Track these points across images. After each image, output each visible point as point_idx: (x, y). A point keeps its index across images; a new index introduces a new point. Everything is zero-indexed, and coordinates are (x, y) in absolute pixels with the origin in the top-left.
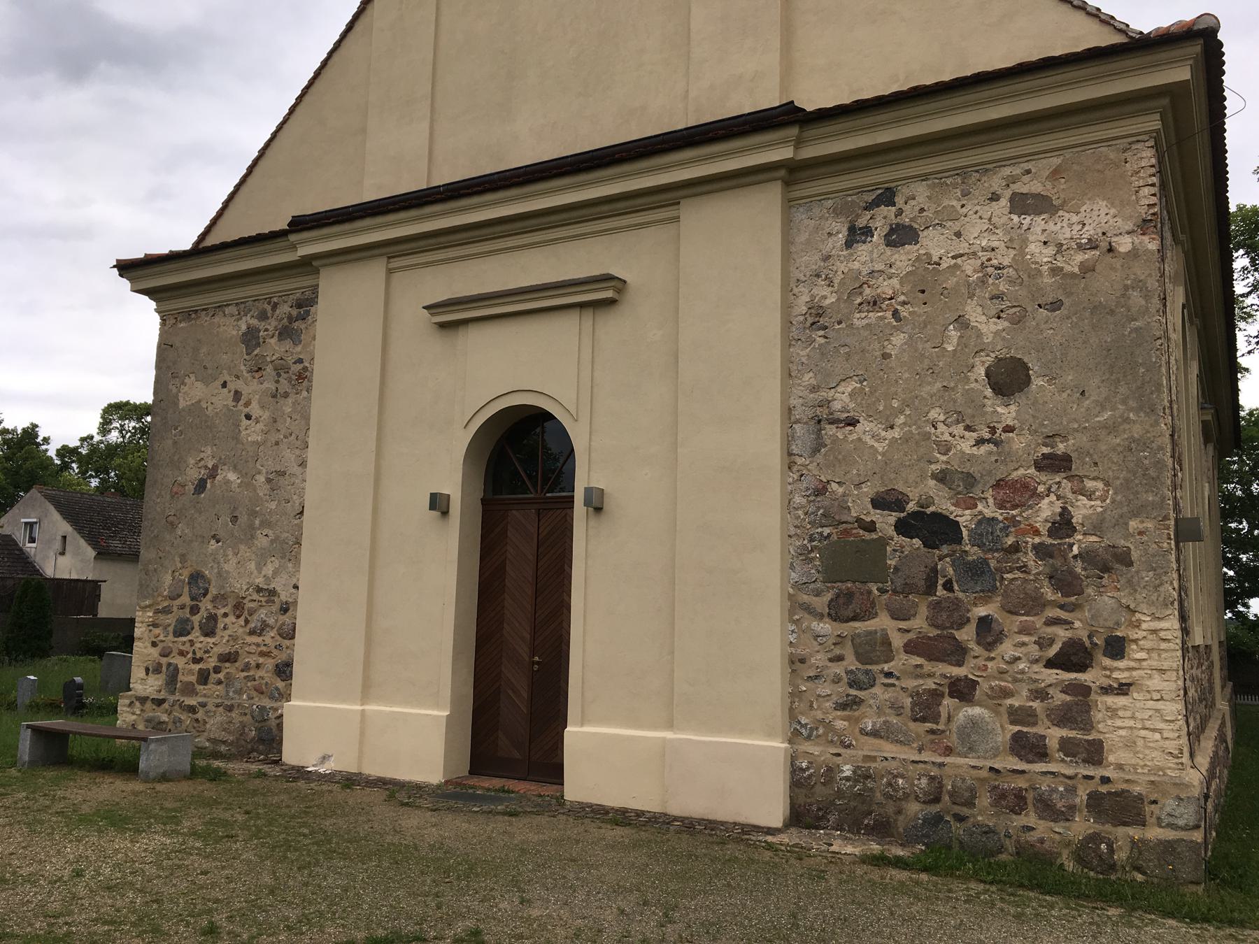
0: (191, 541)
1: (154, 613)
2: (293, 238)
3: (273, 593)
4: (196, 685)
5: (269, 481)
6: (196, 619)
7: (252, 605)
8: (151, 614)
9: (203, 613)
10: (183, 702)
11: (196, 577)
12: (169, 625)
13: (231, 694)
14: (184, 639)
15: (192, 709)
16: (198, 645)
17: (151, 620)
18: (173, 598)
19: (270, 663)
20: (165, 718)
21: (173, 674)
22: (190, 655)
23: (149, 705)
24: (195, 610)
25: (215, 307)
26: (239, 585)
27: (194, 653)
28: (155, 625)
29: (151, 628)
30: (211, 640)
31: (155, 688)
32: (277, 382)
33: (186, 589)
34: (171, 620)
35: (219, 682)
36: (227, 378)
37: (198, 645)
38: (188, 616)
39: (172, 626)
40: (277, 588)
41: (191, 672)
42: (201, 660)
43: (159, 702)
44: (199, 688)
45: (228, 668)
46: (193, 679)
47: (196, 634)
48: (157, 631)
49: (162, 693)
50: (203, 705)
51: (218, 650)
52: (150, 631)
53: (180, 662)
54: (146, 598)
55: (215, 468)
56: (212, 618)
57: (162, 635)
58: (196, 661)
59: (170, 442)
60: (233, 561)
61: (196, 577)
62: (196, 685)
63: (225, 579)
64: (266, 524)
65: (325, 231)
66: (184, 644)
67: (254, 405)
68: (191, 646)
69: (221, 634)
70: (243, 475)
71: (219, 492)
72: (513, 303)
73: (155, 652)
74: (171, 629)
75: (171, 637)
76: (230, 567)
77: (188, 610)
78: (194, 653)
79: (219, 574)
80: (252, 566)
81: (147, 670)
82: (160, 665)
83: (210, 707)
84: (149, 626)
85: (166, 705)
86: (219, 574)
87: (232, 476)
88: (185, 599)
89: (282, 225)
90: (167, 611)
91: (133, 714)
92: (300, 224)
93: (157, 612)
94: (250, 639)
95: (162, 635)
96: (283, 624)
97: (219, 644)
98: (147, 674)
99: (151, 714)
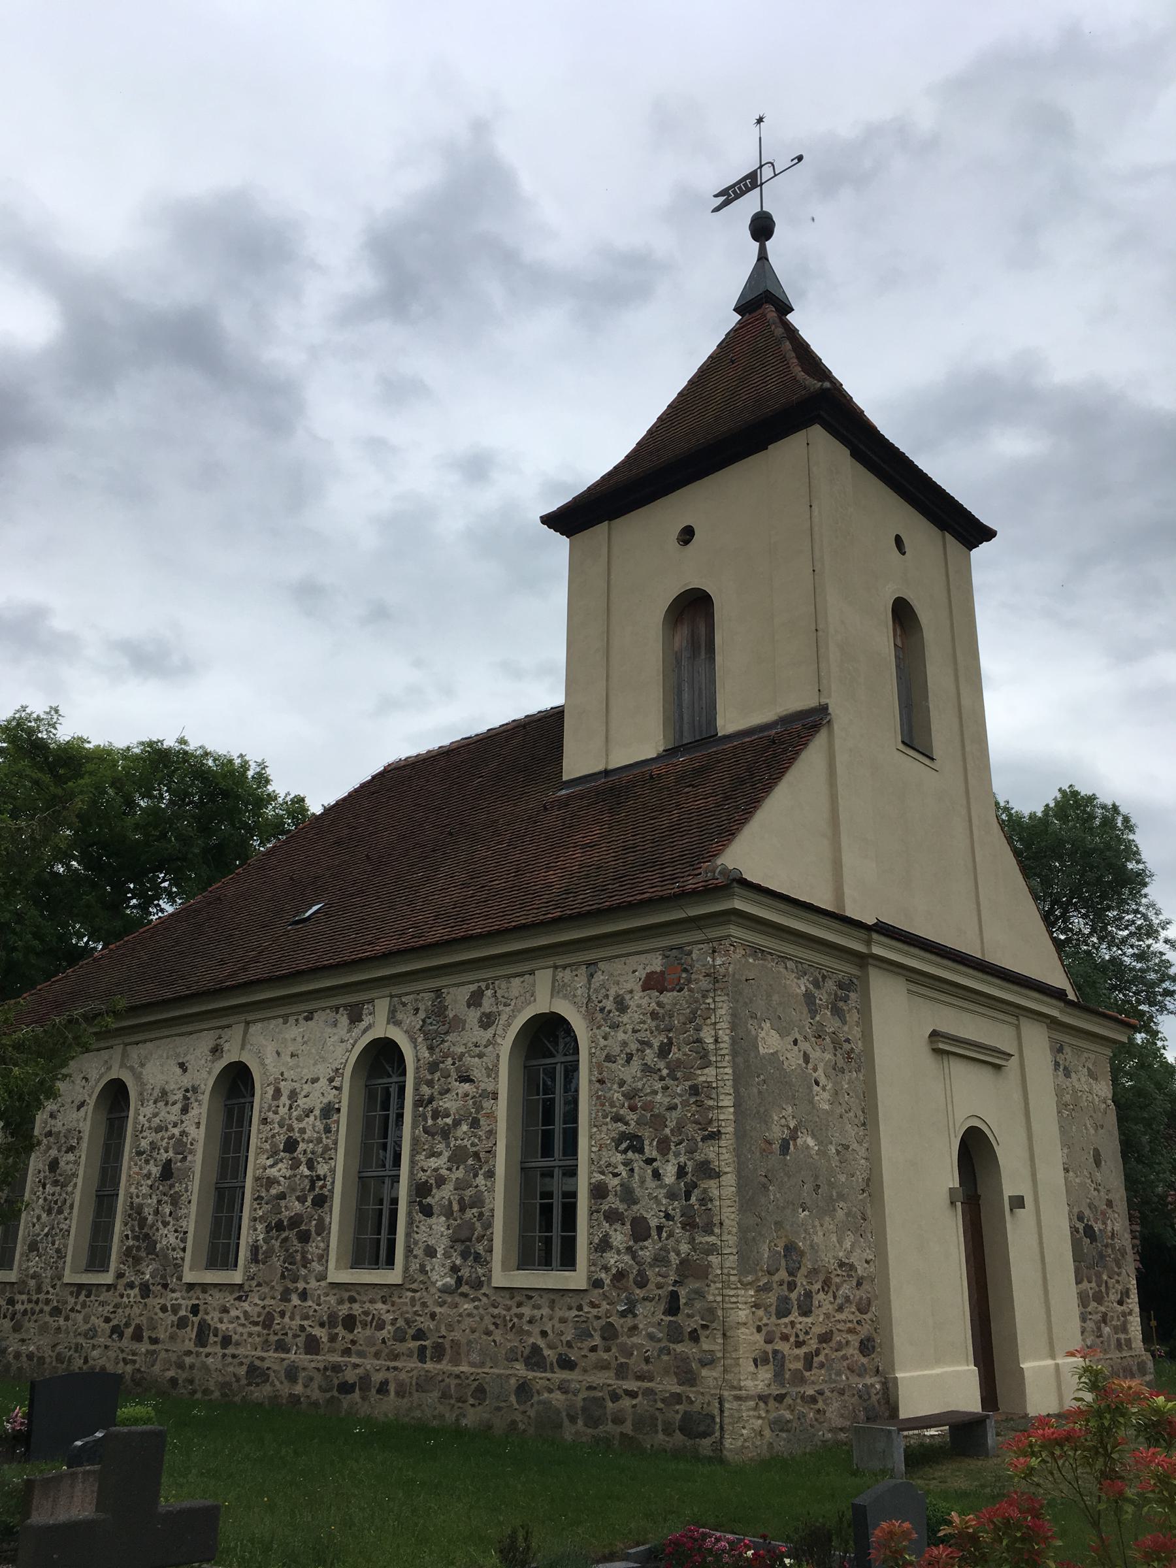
0: (784, 1208)
1: (757, 1291)
2: (875, 936)
3: (852, 1267)
4: (804, 1372)
5: (838, 1152)
6: (794, 1296)
7: (837, 1280)
8: (752, 1292)
9: (799, 1290)
10: (805, 1392)
11: (790, 1248)
12: (771, 1305)
13: (833, 1377)
14: (786, 1320)
15: (813, 1400)
16: (799, 1326)
17: (753, 1299)
18: (771, 1273)
19: (854, 1340)
20: (788, 1415)
21: (778, 1360)
22: (792, 1339)
23: (772, 1403)
24: (792, 1286)
25: (780, 956)
26: (828, 1260)
27: (797, 1336)
28: (756, 1306)
29: (754, 1309)
30: (809, 1320)
31: (766, 1382)
32: (835, 1055)
33: (783, 1263)
34: (771, 1299)
35: (822, 1365)
36: (798, 1036)
37: (799, 1326)
38: (786, 1293)
39: (774, 1307)
40: (855, 1263)
41: (797, 1357)
42: (804, 1343)
43: (780, 1398)
44: (807, 1374)
45: (827, 1350)
46: (799, 1365)
47: (794, 1316)
48: (761, 1312)
49: (773, 1387)
50: (821, 1393)
51: (818, 1330)
52: (753, 1313)
53: (784, 1347)
54: (749, 1273)
55: (796, 1129)
56: (809, 1295)
57: (765, 1318)
58: (799, 1344)
59: (755, 1090)
60: (820, 1233)
61: (790, 1248)
62: (804, 1372)
63: (817, 1252)
64: (841, 1197)
65: (990, 978)
66: (786, 1326)
67: (820, 1071)
68: (793, 1328)
69: (817, 1312)
70: (820, 1143)
71: (802, 1156)
72: (985, 1054)
73: (759, 1338)
74: (773, 1309)
75: (774, 1318)
76: (818, 1239)
77: (785, 1287)
78: (797, 1336)
79: (812, 1246)
80: (834, 1238)
81: (755, 1361)
82: (766, 1353)
83: (828, 1393)
84: (752, 1307)
85: (788, 1400)
86: (812, 1246)
87: (811, 1142)
88: (783, 1274)
89: (871, 921)
90: (767, 1288)
91: (759, 1417)
92: (882, 929)
93: (759, 1290)
94: (839, 1316)
95: (765, 1318)
96: (861, 1298)
97: (816, 1323)
98: (757, 1366)
99: (775, 1414)
